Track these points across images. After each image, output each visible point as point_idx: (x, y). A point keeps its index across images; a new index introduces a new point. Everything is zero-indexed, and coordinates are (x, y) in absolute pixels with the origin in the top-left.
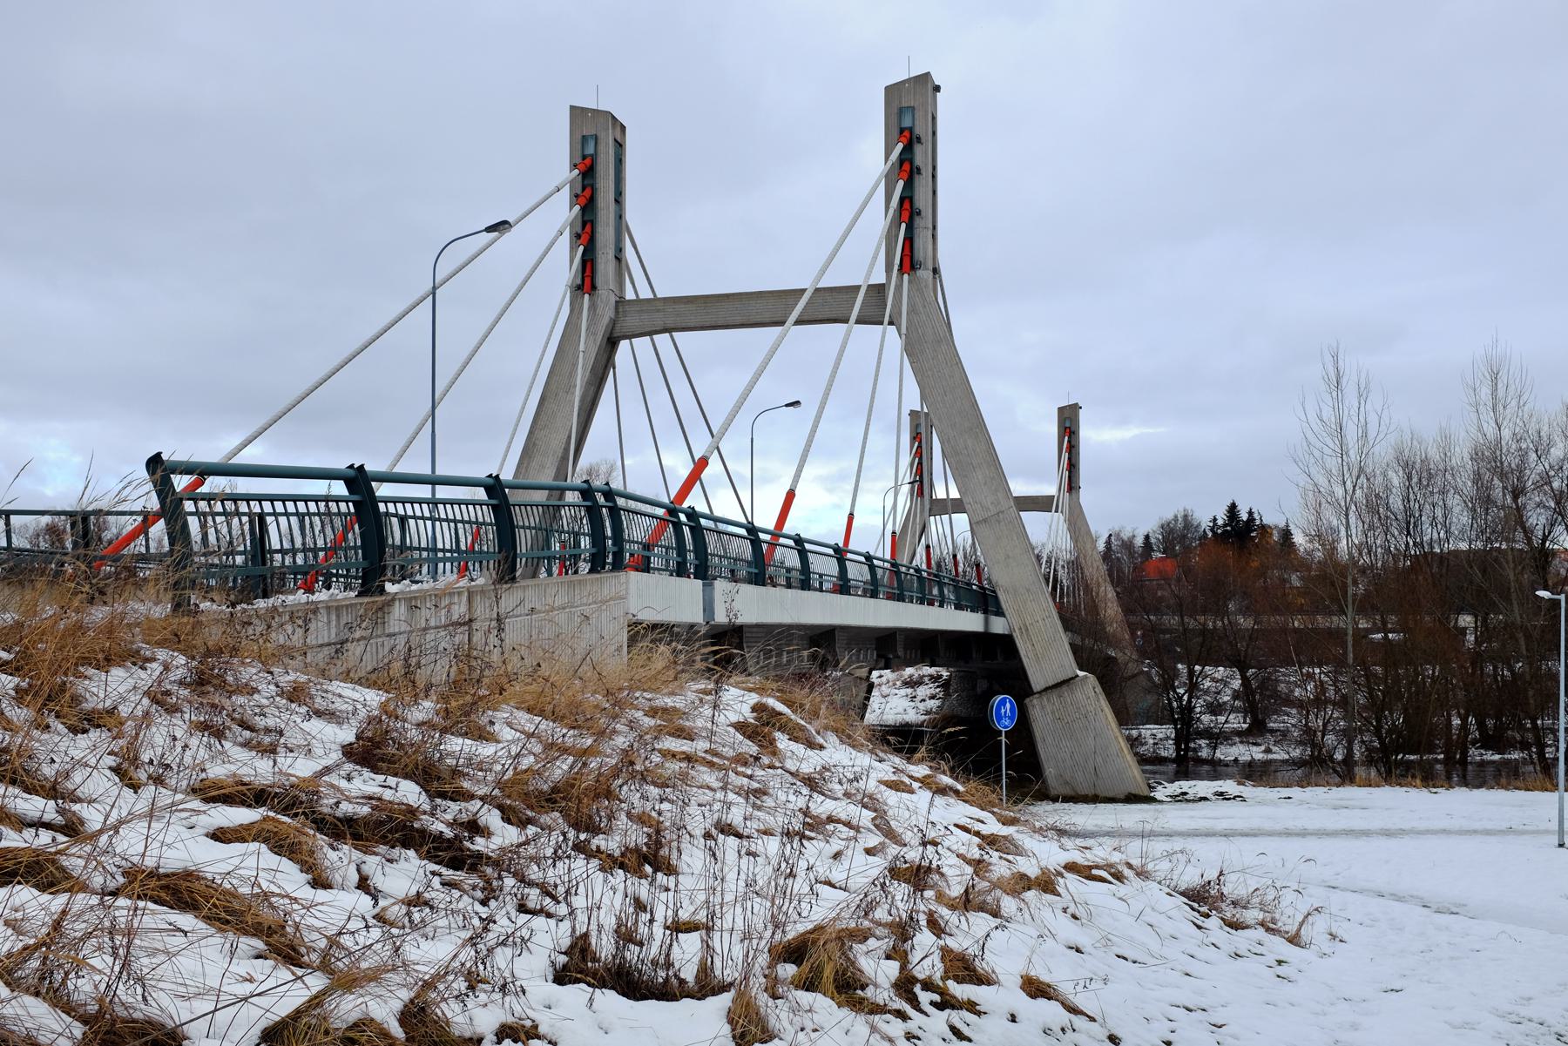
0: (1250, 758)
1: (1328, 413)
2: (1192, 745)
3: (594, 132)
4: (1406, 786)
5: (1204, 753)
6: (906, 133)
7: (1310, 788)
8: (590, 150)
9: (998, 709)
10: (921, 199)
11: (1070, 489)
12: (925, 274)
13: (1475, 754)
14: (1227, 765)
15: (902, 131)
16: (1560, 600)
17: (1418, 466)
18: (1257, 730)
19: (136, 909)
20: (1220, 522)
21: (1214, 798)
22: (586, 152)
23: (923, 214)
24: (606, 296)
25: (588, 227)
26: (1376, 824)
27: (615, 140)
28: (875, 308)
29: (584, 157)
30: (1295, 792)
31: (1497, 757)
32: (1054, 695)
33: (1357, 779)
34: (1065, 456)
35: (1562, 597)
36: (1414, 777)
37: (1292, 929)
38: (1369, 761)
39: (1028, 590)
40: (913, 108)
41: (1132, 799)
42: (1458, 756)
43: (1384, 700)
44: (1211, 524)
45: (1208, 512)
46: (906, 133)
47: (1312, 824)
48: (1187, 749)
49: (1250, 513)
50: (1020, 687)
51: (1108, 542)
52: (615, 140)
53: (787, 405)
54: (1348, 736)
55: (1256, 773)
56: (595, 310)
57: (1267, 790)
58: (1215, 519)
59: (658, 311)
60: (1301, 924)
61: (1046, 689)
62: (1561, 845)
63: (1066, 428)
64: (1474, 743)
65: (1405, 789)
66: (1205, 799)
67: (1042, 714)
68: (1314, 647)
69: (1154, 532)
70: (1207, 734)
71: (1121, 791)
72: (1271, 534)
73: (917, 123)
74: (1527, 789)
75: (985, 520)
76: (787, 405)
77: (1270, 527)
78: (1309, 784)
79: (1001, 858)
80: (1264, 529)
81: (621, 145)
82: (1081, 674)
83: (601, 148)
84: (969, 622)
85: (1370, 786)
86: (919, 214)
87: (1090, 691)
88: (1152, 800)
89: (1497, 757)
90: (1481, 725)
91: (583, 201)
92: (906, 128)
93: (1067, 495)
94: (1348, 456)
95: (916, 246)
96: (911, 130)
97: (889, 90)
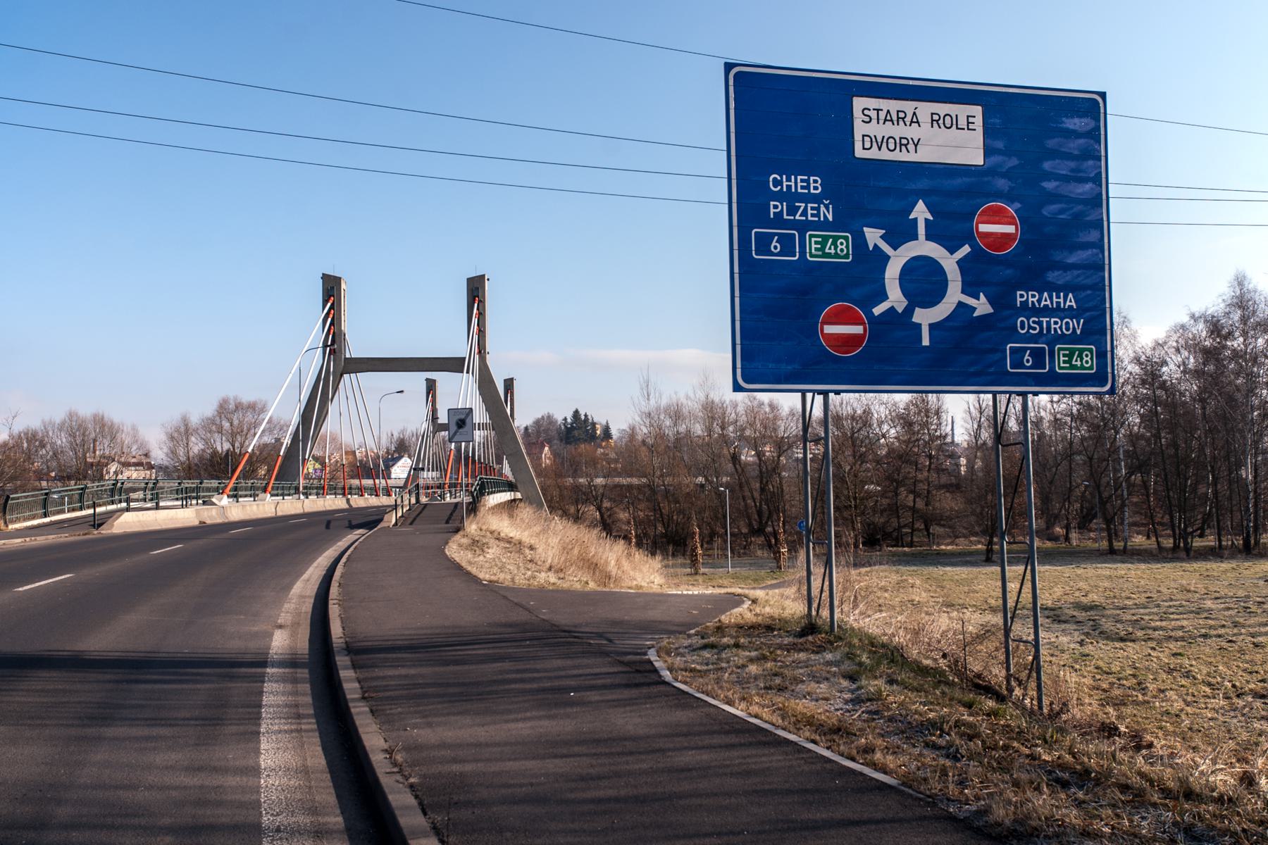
16: (787, 215)
19: (268, 732)
20: (569, 421)
49: (586, 415)
58: (565, 419)
79: (1049, 638)
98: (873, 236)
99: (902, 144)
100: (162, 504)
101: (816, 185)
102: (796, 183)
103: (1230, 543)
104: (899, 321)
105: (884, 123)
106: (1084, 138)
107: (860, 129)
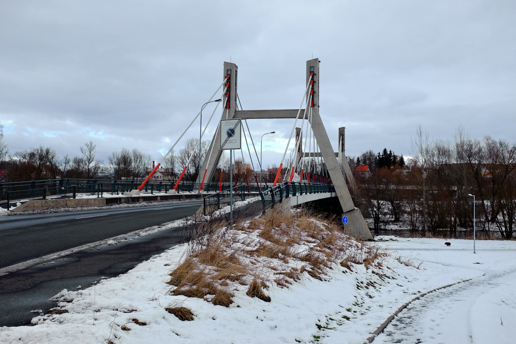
0: (395, 229)
1: (418, 142)
2: (379, 225)
3: (230, 69)
4: (439, 238)
5: (382, 227)
6: (312, 73)
7: (414, 238)
8: (229, 73)
9: (344, 219)
10: (316, 89)
11: (313, 105)
12: (316, 107)
13: (459, 229)
14: (389, 231)
15: (311, 72)
17: (442, 149)
18: (397, 220)
20: (381, 154)
21: (390, 240)
22: (228, 74)
23: (316, 93)
24: (232, 109)
25: (228, 93)
26: (432, 248)
27: (236, 71)
28: (302, 114)
29: (228, 75)
30: (410, 239)
31: (464, 230)
32: (349, 214)
33: (426, 236)
35: (474, 196)
36: (441, 235)
37: (417, 266)
38: (429, 231)
39: (342, 187)
40: (314, 67)
41: (370, 240)
42: (454, 229)
44: (378, 155)
45: (377, 151)
46: (312, 73)
47: (416, 247)
48: (378, 226)
49: (390, 152)
52: (236, 71)
53: (271, 133)
54: (423, 222)
55: (396, 233)
56: (230, 113)
57: (403, 238)
59: (246, 114)
60: (419, 265)
61: (347, 212)
62: (474, 253)
63: (341, 134)
64: (458, 226)
65: (439, 239)
66: (388, 240)
68: (413, 196)
69: (361, 157)
70: (383, 222)
72: (397, 158)
73: (315, 70)
74: (470, 239)
75: (331, 169)
76: (271, 133)
77: (396, 156)
78: (414, 237)
80: (395, 157)
83: (232, 72)
84: (327, 195)
85: (430, 238)
86: (315, 93)
87: (358, 213)
88: (374, 241)
89: (464, 230)
90: (460, 221)
91: (228, 86)
92: (312, 72)
93: (341, 152)
94: (423, 153)
95: (314, 101)
96: (313, 72)
100: (264, 186)
103: (477, 162)
105: (357, 285)
106: (261, 292)
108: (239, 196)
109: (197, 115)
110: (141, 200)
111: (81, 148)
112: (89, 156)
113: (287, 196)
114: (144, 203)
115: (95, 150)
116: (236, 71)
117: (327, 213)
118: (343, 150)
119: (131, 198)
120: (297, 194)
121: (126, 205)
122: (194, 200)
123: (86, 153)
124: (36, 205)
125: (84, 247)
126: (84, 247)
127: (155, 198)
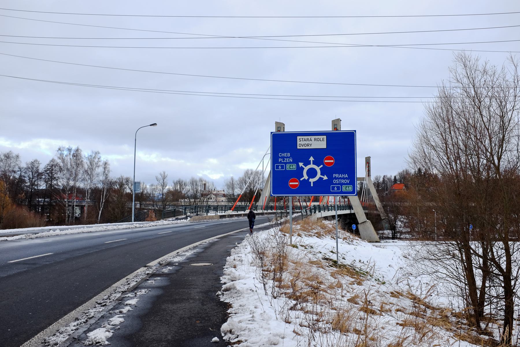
11: (368, 176)
15: (335, 128)
32: (363, 224)
34: (367, 168)
41: (376, 242)
43: (427, 223)
50: (357, 223)
51: (384, 178)
67: (360, 227)
70: (399, 232)
71: (375, 241)
81: (370, 242)
82: (367, 220)
84: (347, 212)
87: (369, 224)
93: (368, 177)
96: (336, 128)
97: (332, 121)
98: (301, 164)
99: (308, 145)
101: (289, 155)
102: (285, 155)
104: (307, 182)
107: (298, 143)
108: (395, 196)
109: (261, 161)
110: (234, 216)
111: (156, 177)
112: (162, 184)
113: (315, 212)
114: (236, 218)
115: (167, 178)
116: (284, 128)
117: (491, 270)
118: (369, 175)
119: (230, 215)
120: (321, 212)
121: (228, 219)
122: (261, 216)
123: (161, 181)
124: (196, 218)
125: (242, 230)
126: (242, 230)
127: (240, 215)
